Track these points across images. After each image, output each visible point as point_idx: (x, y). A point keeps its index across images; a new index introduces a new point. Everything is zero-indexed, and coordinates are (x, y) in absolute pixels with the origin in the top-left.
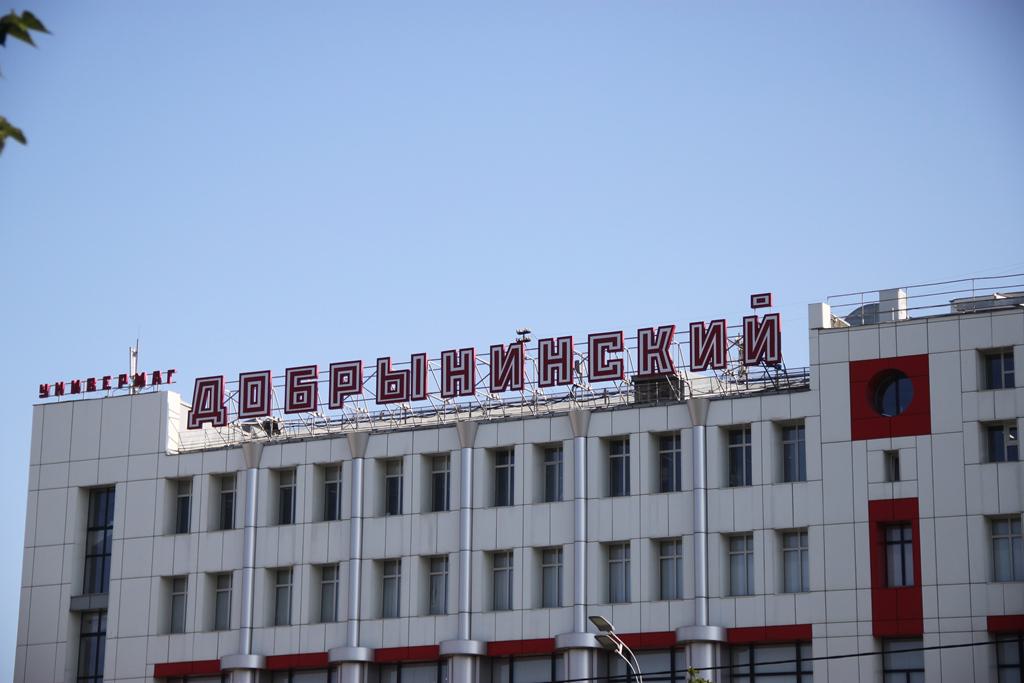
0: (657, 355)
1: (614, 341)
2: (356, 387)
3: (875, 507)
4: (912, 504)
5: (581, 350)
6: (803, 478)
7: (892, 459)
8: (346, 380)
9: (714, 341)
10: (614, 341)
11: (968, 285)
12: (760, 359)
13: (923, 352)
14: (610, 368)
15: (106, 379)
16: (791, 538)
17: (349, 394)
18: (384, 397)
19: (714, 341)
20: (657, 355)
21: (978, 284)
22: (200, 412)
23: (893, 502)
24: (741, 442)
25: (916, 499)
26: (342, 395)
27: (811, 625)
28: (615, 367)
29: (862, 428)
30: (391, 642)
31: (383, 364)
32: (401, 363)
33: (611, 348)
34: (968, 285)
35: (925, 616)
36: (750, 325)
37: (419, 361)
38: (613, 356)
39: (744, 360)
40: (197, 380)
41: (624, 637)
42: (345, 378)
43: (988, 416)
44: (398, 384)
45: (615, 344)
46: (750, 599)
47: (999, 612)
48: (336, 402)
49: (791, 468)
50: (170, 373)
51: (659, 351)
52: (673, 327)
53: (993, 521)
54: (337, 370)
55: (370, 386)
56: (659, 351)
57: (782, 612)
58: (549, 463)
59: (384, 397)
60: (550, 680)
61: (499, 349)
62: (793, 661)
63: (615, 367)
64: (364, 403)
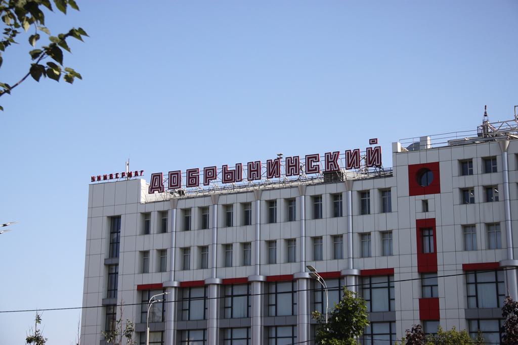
0: (333, 163)
1: (316, 158)
2: (214, 177)
4: (433, 221)
5: (302, 162)
6: (390, 211)
7: (425, 203)
8: (210, 173)
9: (376, 155)
10: (316, 158)
11: (454, 135)
12: (373, 164)
13: (411, 197)
14: (314, 168)
15: (117, 174)
16: (386, 235)
17: (211, 180)
18: (225, 181)
19: (376, 155)
20: (333, 163)
21: (458, 134)
22: (153, 187)
24: (366, 197)
25: (434, 219)
26: (209, 180)
27: (417, 221)
28: (316, 168)
29: (413, 191)
30: (229, 276)
31: (225, 168)
32: (232, 167)
33: (314, 161)
34: (454, 135)
35: (436, 225)
36: (369, 151)
37: (239, 166)
38: (315, 164)
39: (367, 165)
40: (306, 156)
41: (320, 274)
42: (210, 173)
43: (463, 186)
44: (231, 175)
45: (316, 159)
46: (370, 258)
47: (467, 262)
48: (206, 183)
49: (386, 207)
50: (142, 172)
51: (333, 161)
52: (339, 152)
53: (465, 227)
54: (207, 170)
55: (220, 176)
56: (333, 161)
57: (382, 263)
58: (291, 206)
59: (225, 181)
61: (270, 161)
62: (245, 339)
63: (316, 168)
64: (217, 183)
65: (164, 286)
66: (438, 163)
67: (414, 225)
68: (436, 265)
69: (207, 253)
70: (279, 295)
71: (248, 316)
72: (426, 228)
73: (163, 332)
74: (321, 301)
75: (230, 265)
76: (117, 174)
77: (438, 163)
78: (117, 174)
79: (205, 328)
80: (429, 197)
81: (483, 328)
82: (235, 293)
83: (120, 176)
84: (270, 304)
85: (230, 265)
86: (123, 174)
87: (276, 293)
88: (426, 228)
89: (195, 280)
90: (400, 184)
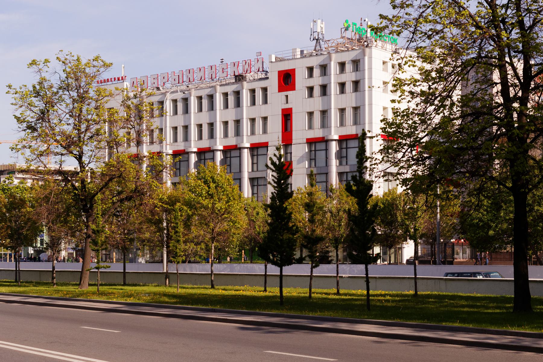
3: (283, 110)
15: (111, 79)
23: (287, 91)
25: (291, 109)
29: (281, 89)
50: (125, 77)
60: (283, 267)
65: (326, 139)
66: (294, 69)
67: (280, 113)
68: (291, 140)
69: (326, 115)
70: (317, 152)
71: (326, 165)
72: (287, 115)
73: (327, 174)
74: (345, 156)
75: (326, 126)
76: (108, 79)
77: (294, 69)
78: (111, 79)
79: (327, 172)
80: (290, 93)
81: (260, 183)
82: (232, 156)
83: (113, 80)
84: (342, 156)
85: (326, 126)
86: (115, 79)
87: (230, 157)
88: (287, 115)
89: (348, 134)
90: (273, 83)
